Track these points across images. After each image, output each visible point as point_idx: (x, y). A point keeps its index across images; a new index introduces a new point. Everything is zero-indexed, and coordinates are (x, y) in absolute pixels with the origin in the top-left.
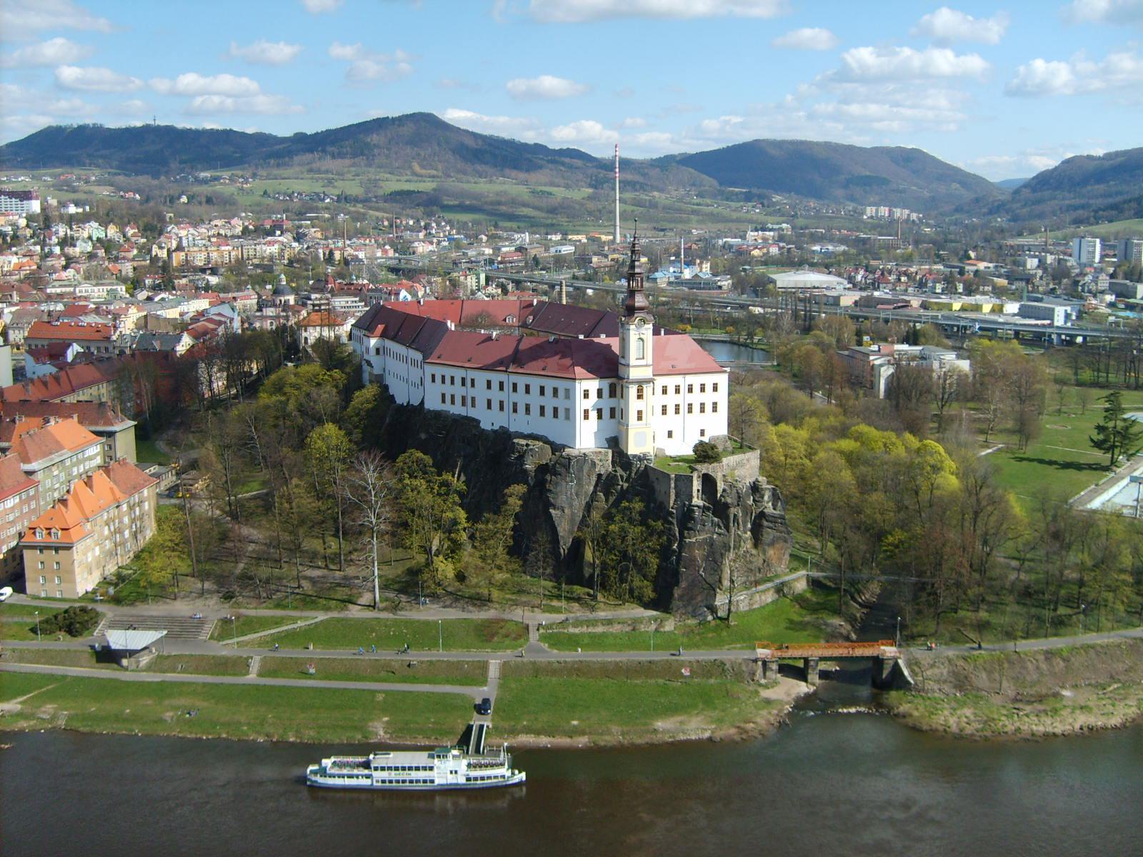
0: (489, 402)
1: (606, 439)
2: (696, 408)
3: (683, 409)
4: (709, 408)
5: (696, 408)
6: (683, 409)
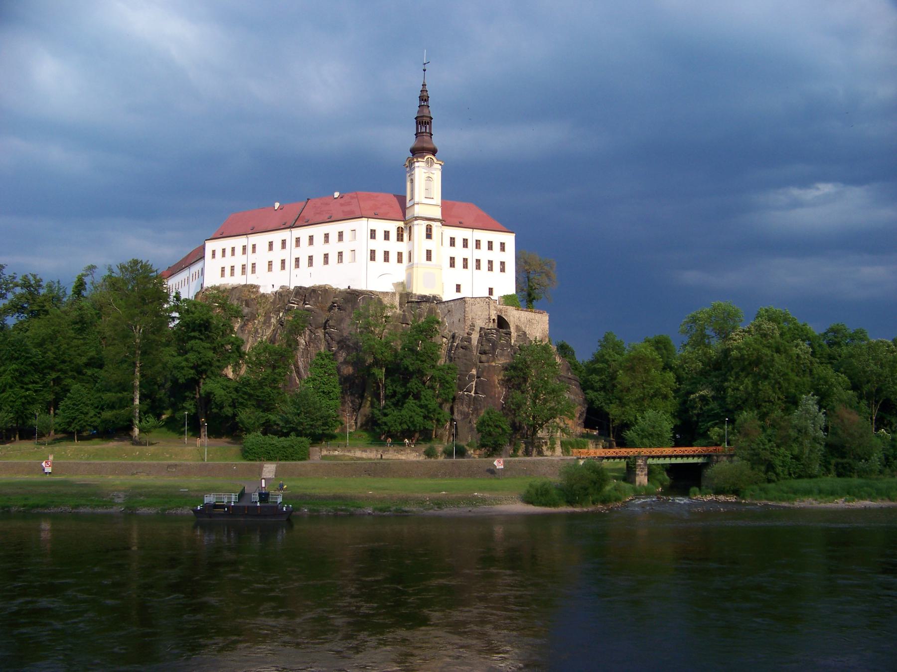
0: (373, 252)
1: (393, 284)
6: (472, 264)
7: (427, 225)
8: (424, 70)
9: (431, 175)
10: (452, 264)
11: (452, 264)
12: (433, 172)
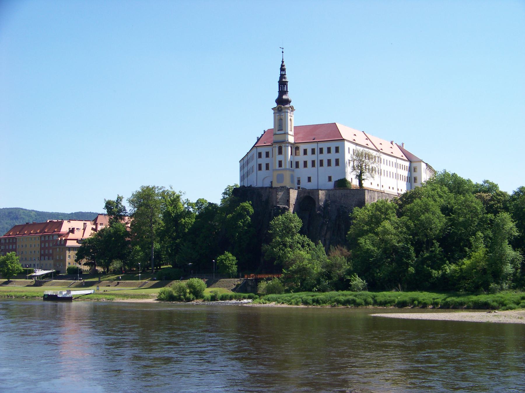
2: (325, 163)
3: (317, 164)
4: (333, 163)
5: (325, 163)
6: (317, 164)
7: (279, 147)
8: (283, 52)
9: (281, 117)
10: (260, 168)
11: (260, 168)
12: (282, 114)
